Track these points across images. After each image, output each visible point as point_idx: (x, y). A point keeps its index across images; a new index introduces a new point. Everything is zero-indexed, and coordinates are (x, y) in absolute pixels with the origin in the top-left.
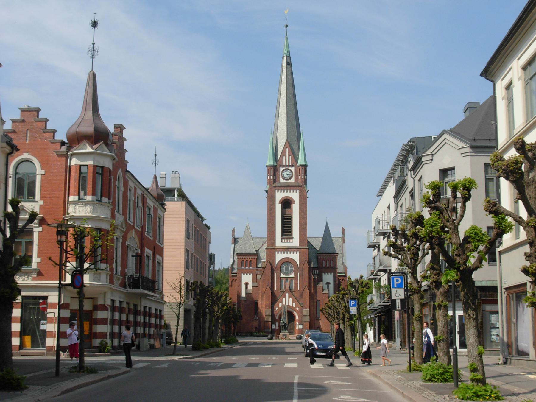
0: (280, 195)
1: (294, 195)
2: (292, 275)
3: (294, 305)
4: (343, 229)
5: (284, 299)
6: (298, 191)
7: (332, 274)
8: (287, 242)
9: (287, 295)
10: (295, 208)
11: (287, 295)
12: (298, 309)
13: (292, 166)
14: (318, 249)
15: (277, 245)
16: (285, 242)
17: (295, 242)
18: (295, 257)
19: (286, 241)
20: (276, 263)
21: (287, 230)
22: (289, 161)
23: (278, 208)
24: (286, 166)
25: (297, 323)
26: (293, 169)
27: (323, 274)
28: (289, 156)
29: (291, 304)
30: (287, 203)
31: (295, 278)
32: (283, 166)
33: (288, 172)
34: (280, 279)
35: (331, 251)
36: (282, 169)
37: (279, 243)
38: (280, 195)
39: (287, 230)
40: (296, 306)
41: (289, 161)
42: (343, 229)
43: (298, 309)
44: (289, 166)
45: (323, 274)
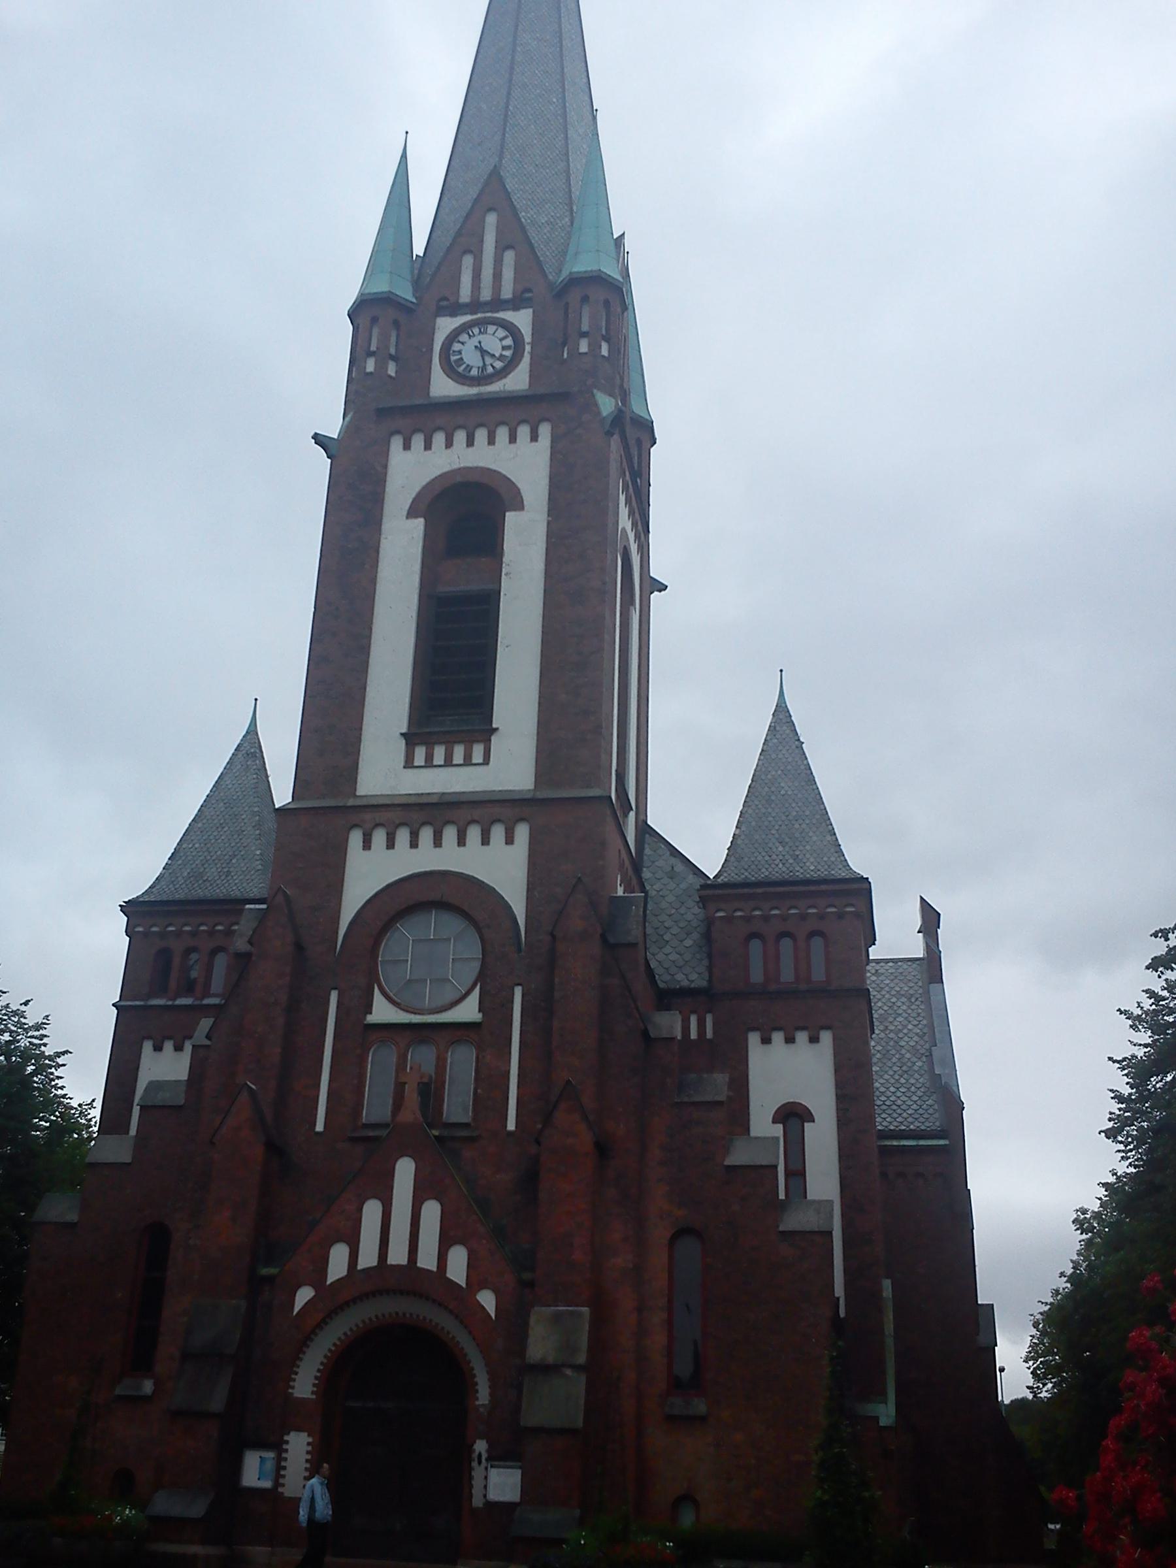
0: (412, 468)
1: (523, 461)
2: (468, 1011)
3: (458, 1267)
4: (925, 906)
5: (372, 1211)
6: (545, 430)
7: (826, 1037)
8: (448, 762)
9: (405, 1171)
10: (525, 542)
11: (405, 1171)
12: (487, 1300)
13: (516, 303)
14: (711, 866)
15: (361, 790)
16: (429, 763)
17: (510, 761)
18: (501, 865)
19: (439, 753)
20: (493, 1316)
21: (453, 699)
22: (497, 276)
23: (402, 546)
24: (475, 306)
25: (481, 1446)
26: (523, 319)
27: (754, 1038)
28: (502, 247)
29: (427, 1260)
30: (466, 517)
31: (485, 1035)
32: (455, 309)
33: (495, 341)
34: (360, 1035)
35: (811, 868)
36: (446, 325)
37: (384, 768)
38: (412, 468)
39: (453, 699)
40: (477, 1280)
41: (497, 276)
42: (925, 906)
43: (487, 1300)
44: (498, 303)
45: (754, 1038)
